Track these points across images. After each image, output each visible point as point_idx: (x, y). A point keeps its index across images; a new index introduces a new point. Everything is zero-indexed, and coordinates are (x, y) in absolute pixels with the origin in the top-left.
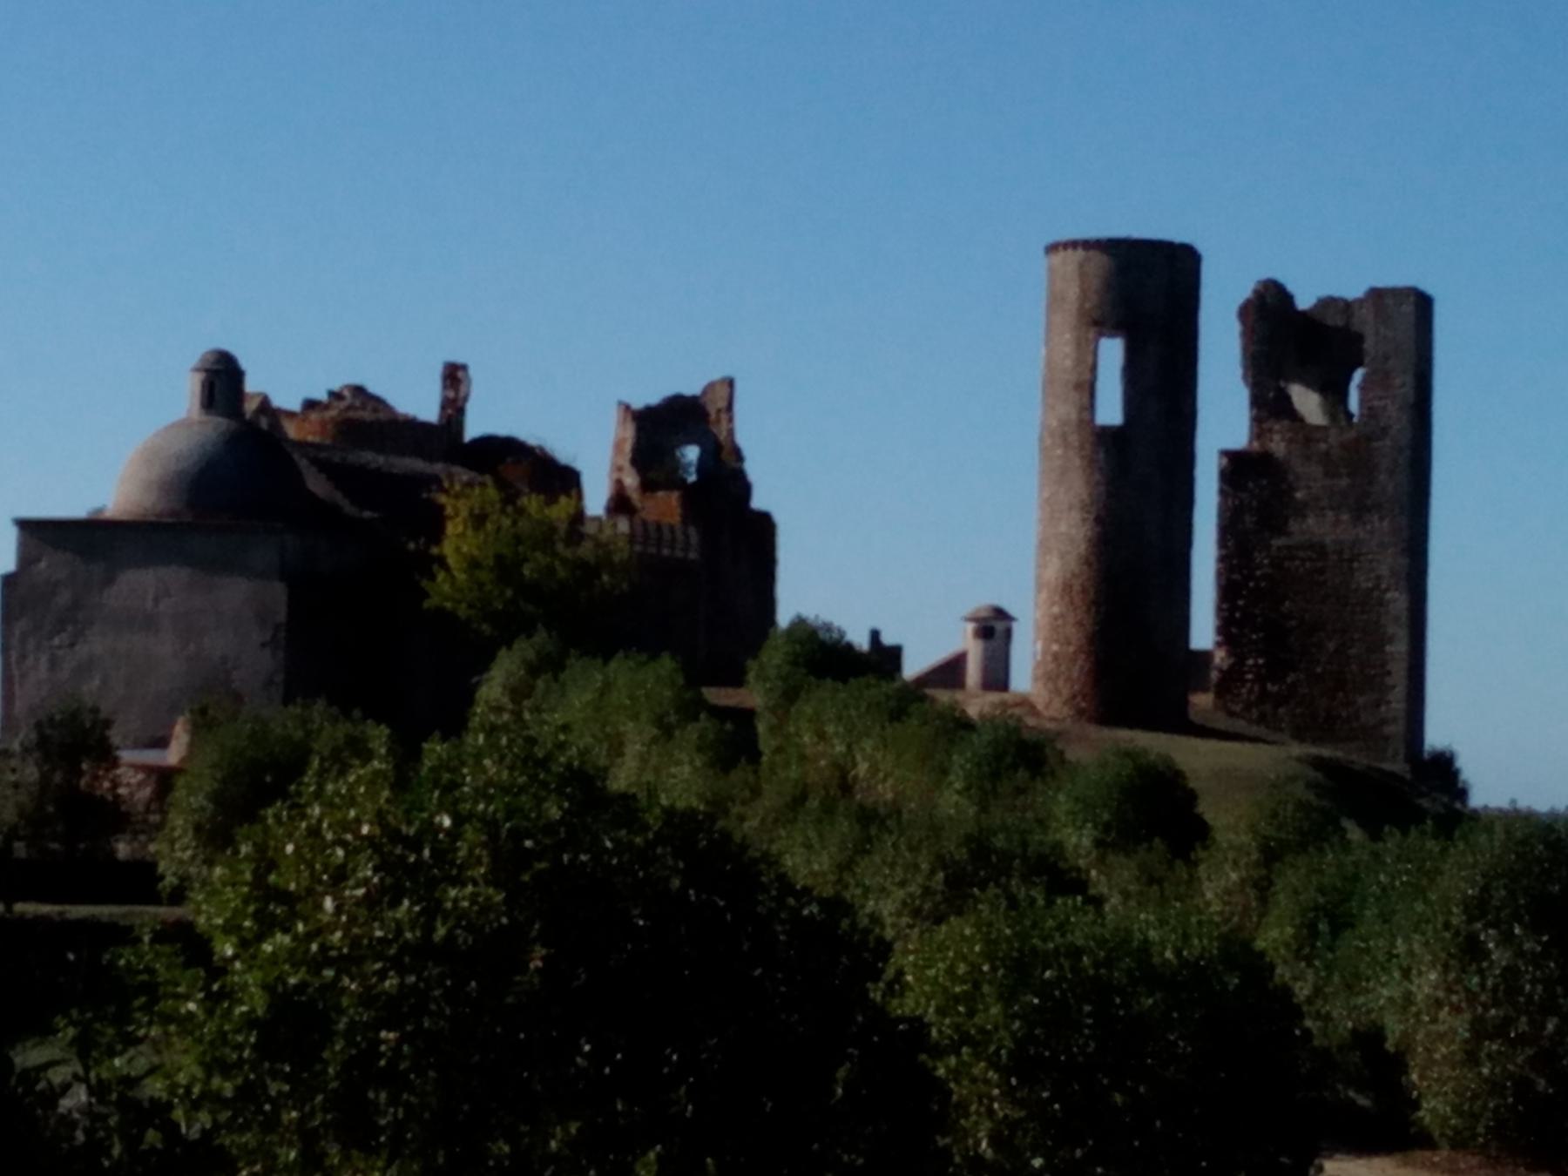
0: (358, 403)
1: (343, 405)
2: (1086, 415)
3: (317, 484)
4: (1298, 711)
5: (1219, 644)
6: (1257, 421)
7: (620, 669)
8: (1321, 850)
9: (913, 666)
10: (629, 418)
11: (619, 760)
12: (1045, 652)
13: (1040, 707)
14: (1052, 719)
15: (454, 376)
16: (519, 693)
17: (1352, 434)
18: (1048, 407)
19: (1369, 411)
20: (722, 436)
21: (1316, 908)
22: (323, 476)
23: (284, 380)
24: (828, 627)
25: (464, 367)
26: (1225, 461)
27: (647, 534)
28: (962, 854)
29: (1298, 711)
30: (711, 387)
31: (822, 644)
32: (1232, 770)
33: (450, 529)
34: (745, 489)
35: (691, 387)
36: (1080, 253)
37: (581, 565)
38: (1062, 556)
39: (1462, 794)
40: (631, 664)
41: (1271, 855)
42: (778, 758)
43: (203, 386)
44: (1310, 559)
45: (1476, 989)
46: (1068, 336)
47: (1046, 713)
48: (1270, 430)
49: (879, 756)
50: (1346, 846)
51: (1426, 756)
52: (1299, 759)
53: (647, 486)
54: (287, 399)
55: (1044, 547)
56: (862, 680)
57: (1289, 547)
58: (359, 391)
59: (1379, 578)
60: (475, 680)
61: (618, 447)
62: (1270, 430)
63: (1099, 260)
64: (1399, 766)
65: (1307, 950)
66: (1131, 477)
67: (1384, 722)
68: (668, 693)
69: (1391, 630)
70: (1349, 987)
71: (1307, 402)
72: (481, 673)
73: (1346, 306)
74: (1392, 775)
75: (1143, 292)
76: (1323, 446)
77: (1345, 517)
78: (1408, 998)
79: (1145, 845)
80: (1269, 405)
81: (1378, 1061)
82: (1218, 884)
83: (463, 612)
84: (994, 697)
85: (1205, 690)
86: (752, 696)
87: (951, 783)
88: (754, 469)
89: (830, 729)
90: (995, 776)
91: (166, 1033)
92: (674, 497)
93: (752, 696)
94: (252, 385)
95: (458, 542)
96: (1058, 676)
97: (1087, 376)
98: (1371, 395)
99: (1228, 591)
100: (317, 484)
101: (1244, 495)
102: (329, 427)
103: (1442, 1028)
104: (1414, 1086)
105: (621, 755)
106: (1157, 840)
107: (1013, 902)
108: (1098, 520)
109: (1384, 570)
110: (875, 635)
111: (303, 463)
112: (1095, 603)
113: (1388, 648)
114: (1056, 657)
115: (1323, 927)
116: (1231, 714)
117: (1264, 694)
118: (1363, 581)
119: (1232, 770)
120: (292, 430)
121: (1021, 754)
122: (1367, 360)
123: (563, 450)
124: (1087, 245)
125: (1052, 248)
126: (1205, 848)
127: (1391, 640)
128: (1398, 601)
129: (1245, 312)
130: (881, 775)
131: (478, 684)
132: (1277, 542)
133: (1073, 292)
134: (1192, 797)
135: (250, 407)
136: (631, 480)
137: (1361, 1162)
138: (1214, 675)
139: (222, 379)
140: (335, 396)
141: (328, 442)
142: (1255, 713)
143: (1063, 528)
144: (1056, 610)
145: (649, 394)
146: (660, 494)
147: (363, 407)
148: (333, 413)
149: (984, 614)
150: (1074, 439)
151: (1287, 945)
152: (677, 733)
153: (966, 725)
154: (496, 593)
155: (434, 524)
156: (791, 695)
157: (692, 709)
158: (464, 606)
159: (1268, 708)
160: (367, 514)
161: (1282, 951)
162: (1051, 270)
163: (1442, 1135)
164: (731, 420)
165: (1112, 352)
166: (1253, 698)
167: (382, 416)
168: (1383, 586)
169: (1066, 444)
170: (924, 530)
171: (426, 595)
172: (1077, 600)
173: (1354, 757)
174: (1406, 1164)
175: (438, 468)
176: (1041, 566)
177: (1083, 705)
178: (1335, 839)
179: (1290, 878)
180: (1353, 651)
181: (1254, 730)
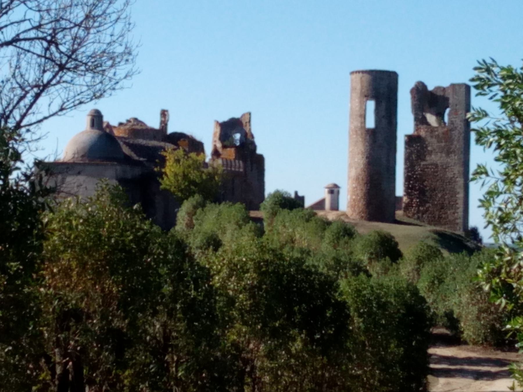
0: (135, 123)
1: (130, 124)
2: (363, 125)
3: (126, 150)
4: (430, 216)
5: (405, 195)
6: (416, 125)
7: (223, 207)
8: (436, 260)
9: (308, 203)
10: (218, 125)
11: (225, 235)
12: (351, 198)
13: (349, 215)
14: (353, 219)
15: (164, 113)
16: (191, 214)
17: (446, 129)
18: (351, 123)
19: (451, 122)
20: (247, 131)
21: (434, 277)
22: (128, 147)
24: (286, 193)
25: (167, 111)
26: (406, 138)
27: (227, 163)
28: (332, 263)
29: (430, 216)
30: (244, 115)
31: (284, 198)
32: (410, 236)
33: (168, 164)
34: (255, 147)
35: (237, 115)
36: (361, 75)
37: (209, 174)
38: (356, 169)
39: (480, 241)
40: (228, 206)
41: (420, 261)
42: (270, 233)
43: (91, 120)
44: (433, 168)
45: (479, 299)
46: (357, 100)
47: (351, 218)
48: (420, 128)
49: (302, 232)
50: (443, 258)
51: (469, 229)
52: (430, 231)
53: (224, 147)
54: (114, 123)
55: (350, 166)
56: (298, 209)
57: (426, 165)
58: (136, 119)
59: (454, 174)
60: (176, 210)
61: (215, 134)
62: (420, 128)
63: (367, 77)
64: (460, 232)
65: (431, 289)
66: (378, 142)
67: (456, 219)
68: (240, 215)
69: (458, 190)
70: (444, 300)
71: (431, 119)
72: (178, 208)
73: (444, 89)
74: (459, 236)
75: (381, 87)
76: (437, 133)
77: (444, 155)
78: (460, 302)
79: (384, 259)
80: (420, 121)
81: (452, 322)
82: (405, 270)
83: (172, 189)
84: (335, 213)
85: (400, 209)
86: (261, 214)
87: (325, 241)
88: (257, 141)
89: (287, 224)
90: (338, 238)
91: (164, 310)
92: (233, 150)
93: (261, 214)
94: (105, 119)
95: (171, 169)
96: (355, 206)
97: (363, 113)
98: (451, 117)
99: (408, 179)
100: (126, 150)
101: (412, 149)
102: (127, 131)
103: (470, 311)
104: (462, 327)
105: (225, 233)
106: (387, 258)
108: (367, 158)
109: (456, 172)
110: (296, 193)
111: (121, 143)
112: (366, 183)
113: (457, 196)
114: (354, 200)
115: (436, 282)
116: (409, 217)
117: (418, 212)
118: (449, 175)
119: (410, 236)
120: (116, 133)
121: (347, 232)
122: (450, 106)
123: (198, 137)
124: (363, 72)
125: (352, 73)
126: (402, 259)
127: (458, 193)
128: (460, 181)
129: (412, 91)
130: (303, 238)
131: (178, 211)
132: (423, 163)
133: (359, 87)
134: (397, 244)
135: (105, 125)
136: (219, 145)
137: (447, 349)
138: (403, 205)
140: (129, 121)
141: (126, 136)
142: (416, 216)
143: (356, 160)
144: (354, 185)
145: (225, 118)
146: (228, 149)
147: (138, 124)
148: (127, 127)
149: (331, 186)
150: (359, 132)
151: (426, 288)
152: (243, 227)
153: (329, 223)
154: (182, 183)
155: (163, 161)
156: (274, 214)
157: (248, 219)
158: (173, 187)
159: (420, 215)
160: (141, 159)
161: (424, 289)
162: (352, 80)
163: (470, 341)
164: (250, 125)
165: (371, 105)
166: (415, 212)
167: (144, 128)
168: (456, 177)
169: (357, 135)
170: (312, 160)
171: (161, 184)
172: (361, 182)
173: (447, 230)
174: (460, 349)
175: (162, 144)
176: (350, 172)
177: (363, 215)
178: (440, 256)
179: (427, 268)
180: (446, 197)
181: (416, 222)
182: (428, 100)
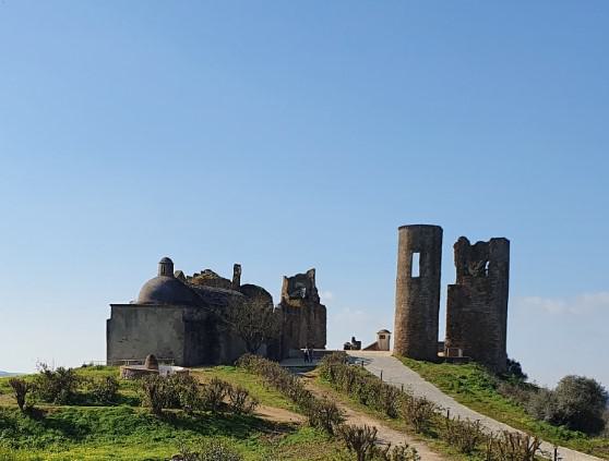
6: (458, 277)
15: (237, 268)
23: (188, 267)
61: (283, 289)
66: (419, 294)
75: (424, 240)
80: (461, 273)
107: (432, 301)
125: (400, 228)
133: (406, 241)
136: (287, 297)
139: (167, 265)
165: (416, 256)
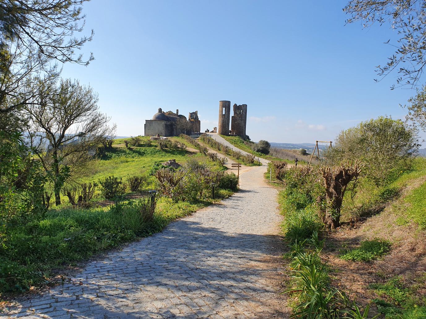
15: (177, 110)
75: (226, 105)
80: (235, 113)
136: (190, 118)
165: (224, 109)
182: (236, 108)
